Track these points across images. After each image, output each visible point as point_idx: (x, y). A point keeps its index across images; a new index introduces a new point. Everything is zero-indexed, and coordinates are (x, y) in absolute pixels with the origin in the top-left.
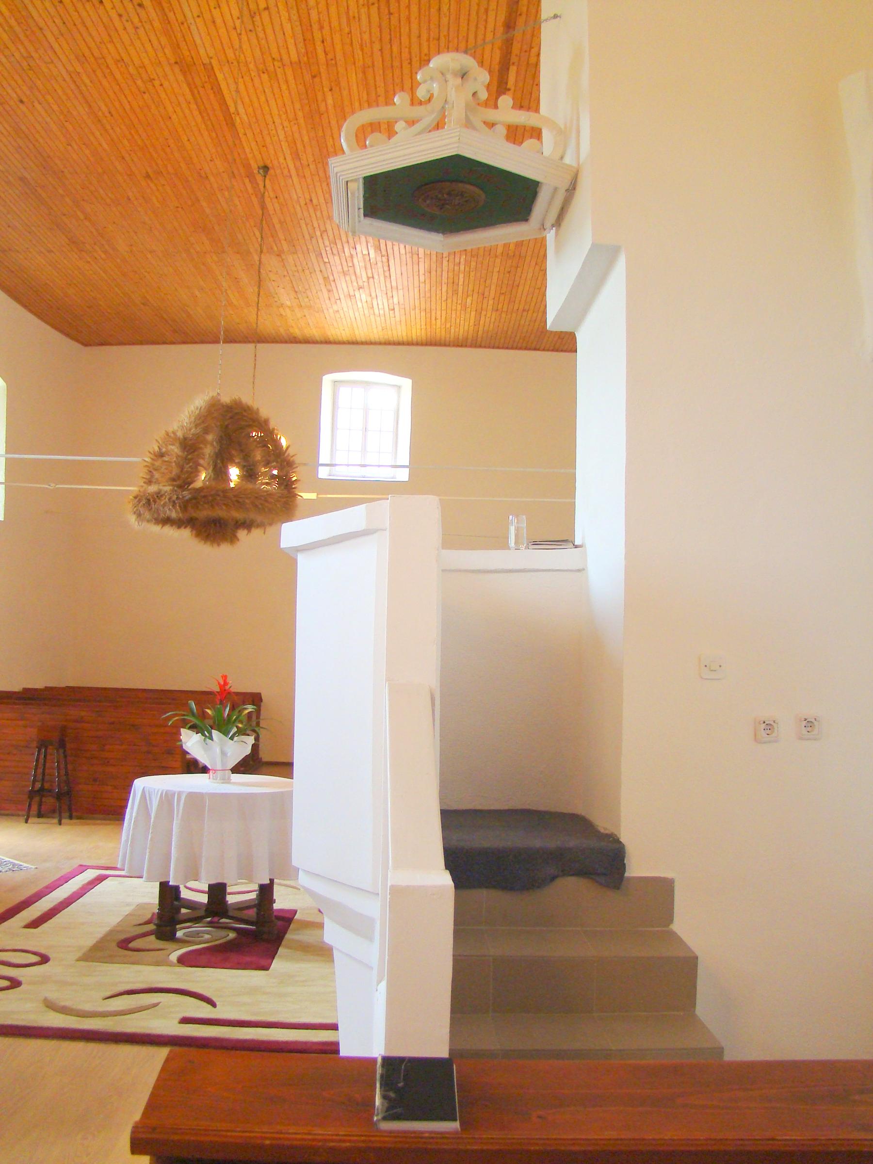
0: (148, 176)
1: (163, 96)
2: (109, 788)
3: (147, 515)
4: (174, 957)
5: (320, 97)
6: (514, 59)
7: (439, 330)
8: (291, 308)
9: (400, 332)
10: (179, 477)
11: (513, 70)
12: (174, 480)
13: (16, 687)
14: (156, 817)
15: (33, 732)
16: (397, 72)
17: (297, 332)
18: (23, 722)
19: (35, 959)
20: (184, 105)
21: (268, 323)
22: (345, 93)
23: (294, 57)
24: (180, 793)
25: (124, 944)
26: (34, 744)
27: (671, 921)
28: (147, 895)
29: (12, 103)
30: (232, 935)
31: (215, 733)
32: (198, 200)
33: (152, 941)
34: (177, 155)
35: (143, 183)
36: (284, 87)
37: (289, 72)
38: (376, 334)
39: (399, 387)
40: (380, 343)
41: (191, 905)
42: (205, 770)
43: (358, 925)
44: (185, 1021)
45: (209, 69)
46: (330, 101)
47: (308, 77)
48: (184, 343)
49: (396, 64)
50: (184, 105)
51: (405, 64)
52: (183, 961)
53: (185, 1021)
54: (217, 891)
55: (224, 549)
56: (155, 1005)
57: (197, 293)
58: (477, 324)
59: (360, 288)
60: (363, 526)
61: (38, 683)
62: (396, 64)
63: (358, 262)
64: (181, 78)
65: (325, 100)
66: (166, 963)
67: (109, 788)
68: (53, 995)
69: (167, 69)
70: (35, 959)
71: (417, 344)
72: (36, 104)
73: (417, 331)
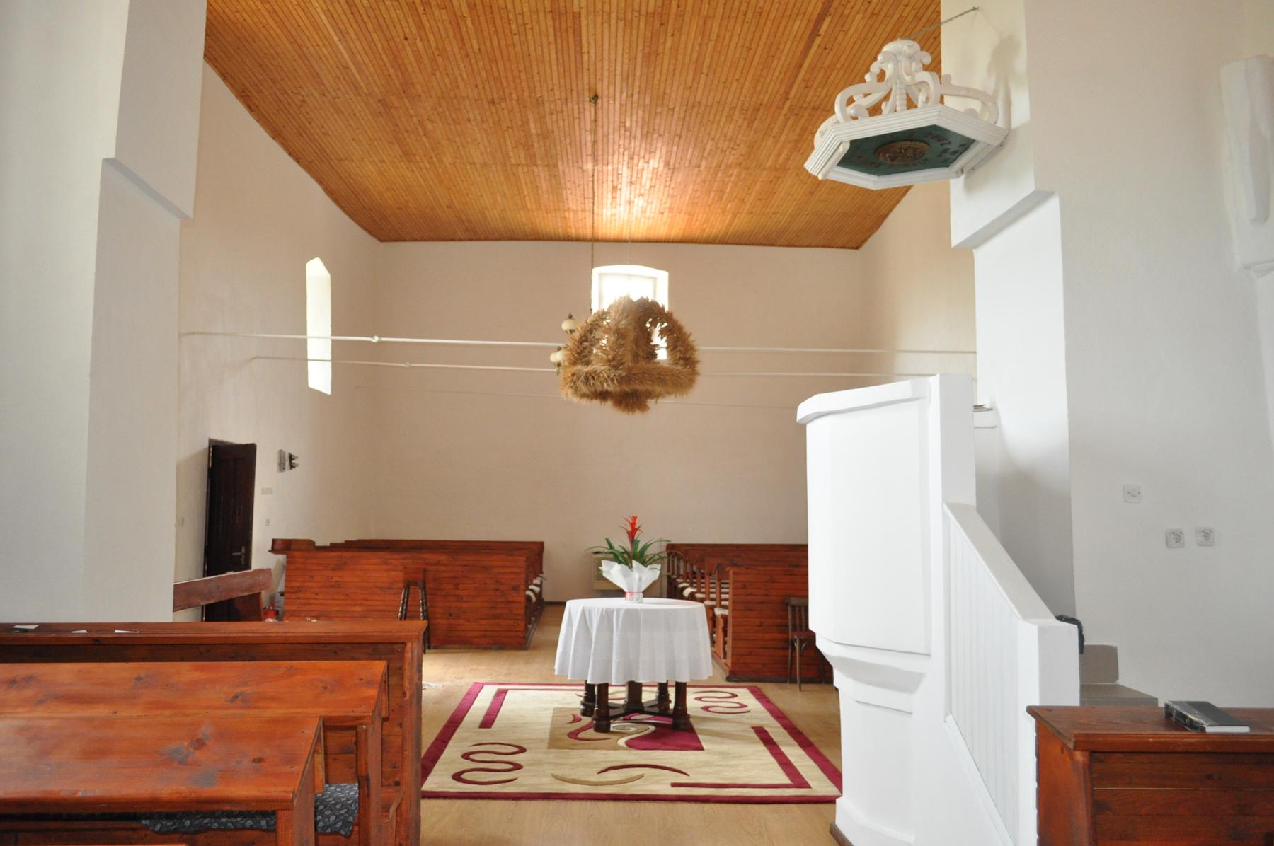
0: (493, 102)
1: (530, 37)
2: (461, 622)
3: (585, 389)
4: (622, 742)
5: (662, 40)
6: (832, 10)
7: (696, 230)
8: (575, 212)
9: (662, 231)
10: (614, 359)
11: (828, 19)
12: (609, 361)
13: (340, 540)
14: (598, 630)
15: (399, 575)
16: (732, 22)
17: (573, 232)
18: (385, 567)
19: (515, 749)
20: (545, 45)
21: (549, 223)
22: (684, 38)
23: (651, 9)
24: (618, 610)
25: (573, 735)
26: (401, 585)
27: (1116, 677)
28: (573, 700)
29: (397, 40)
30: (652, 728)
31: (635, 563)
32: (528, 123)
33: (591, 733)
34: (524, 84)
35: (487, 106)
36: (635, 32)
37: (643, 20)
38: (640, 231)
39: (655, 279)
40: (641, 241)
41: (615, 707)
42: (620, 593)
43: (786, 745)
44: (674, 785)
45: (577, 17)
46: (669, 44)
47: (657, 24)
48: (471, 240)
49: (734, 14)
50: (545, 45)
51: (741, 15)
52: (630, 744)
53: (674, 785)
54: (635, 689)
55: (638, 415)
56: (642, 776)
57: (499, 199)
58: (730, 225)
59: (641, 195)
60: (909, 395)
61: (353, 538)
62: (734, 14)
63: (646, 176)
64: (550, 23)
65: (665, 43)
66: (617, 748)
67: (461, 622)
68: (558, 772)
69: (542, 16)
70: (515, 749)
71: (673, 242)
72: (418, 41)
73: (676, 232)
